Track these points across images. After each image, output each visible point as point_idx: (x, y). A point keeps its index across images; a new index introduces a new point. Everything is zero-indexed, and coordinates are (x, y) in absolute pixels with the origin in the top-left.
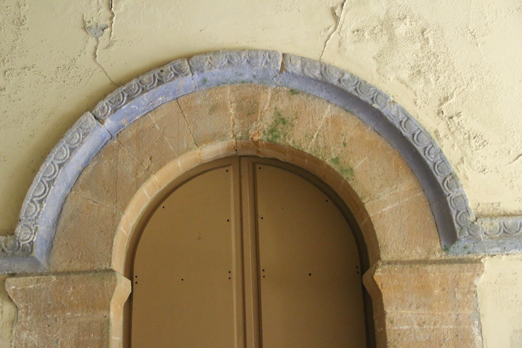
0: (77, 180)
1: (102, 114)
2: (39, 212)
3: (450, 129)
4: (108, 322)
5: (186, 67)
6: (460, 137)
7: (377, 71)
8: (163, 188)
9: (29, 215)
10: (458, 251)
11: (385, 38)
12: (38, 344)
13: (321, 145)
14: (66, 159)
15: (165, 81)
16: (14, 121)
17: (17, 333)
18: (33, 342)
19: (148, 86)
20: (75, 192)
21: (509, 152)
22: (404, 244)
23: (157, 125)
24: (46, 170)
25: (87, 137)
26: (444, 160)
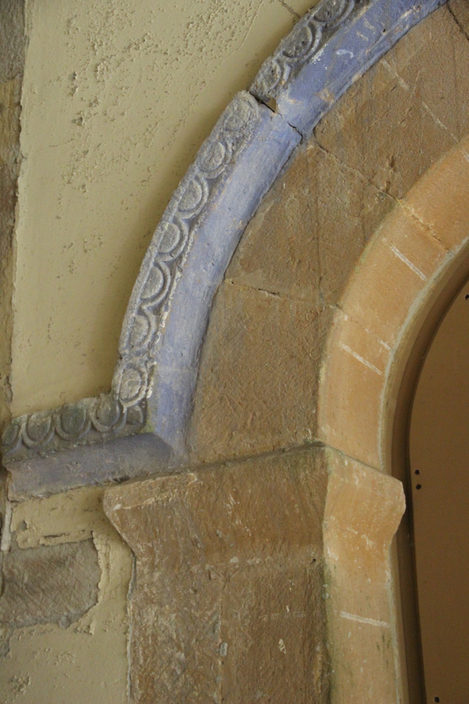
0: (234, 253)
1: (269, 86)
2: (155, 333)
9: (136, 343)
12: (178, 636)
14: (201, 206)
16: (113, 160)
17: (137, 612)
18: (167, 631)
20: (231, 280)
23: (402, 82)
24: (163, 239)
25: (243, 148)
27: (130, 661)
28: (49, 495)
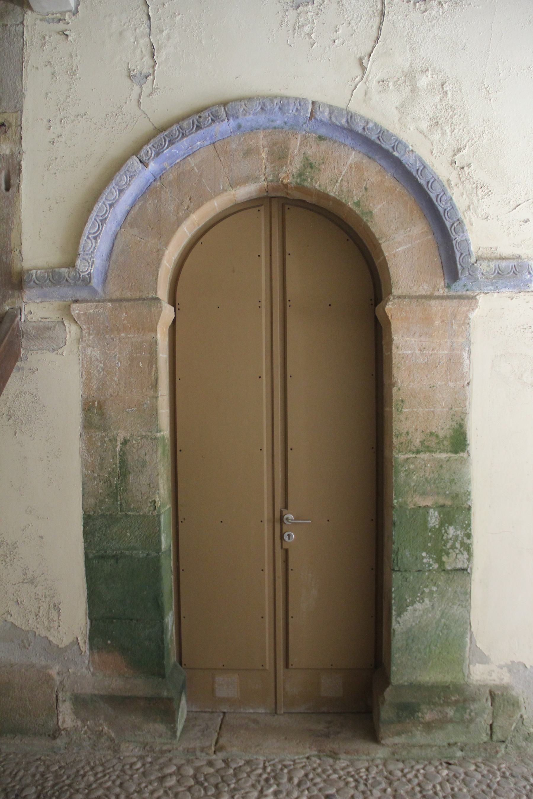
0: (125, 219)
1: (146, 157)
2: (95, 247)
3: (460, 179)
4: (156, 343)
5: (222, 113)
6: (469, 186)
7: (399, 120)
8: (201, 225)
10: (459, 288)
11: (408, 89)
12: (100, 358)
13: (345, 189)
14: (115, 200)
15: (203, 127)
19: (187, 131)
21: (509, 202)
22: (413, 281)
23: (195, 168)
26: (453, 207)
27: (81, 366)
28: (42, 302)
